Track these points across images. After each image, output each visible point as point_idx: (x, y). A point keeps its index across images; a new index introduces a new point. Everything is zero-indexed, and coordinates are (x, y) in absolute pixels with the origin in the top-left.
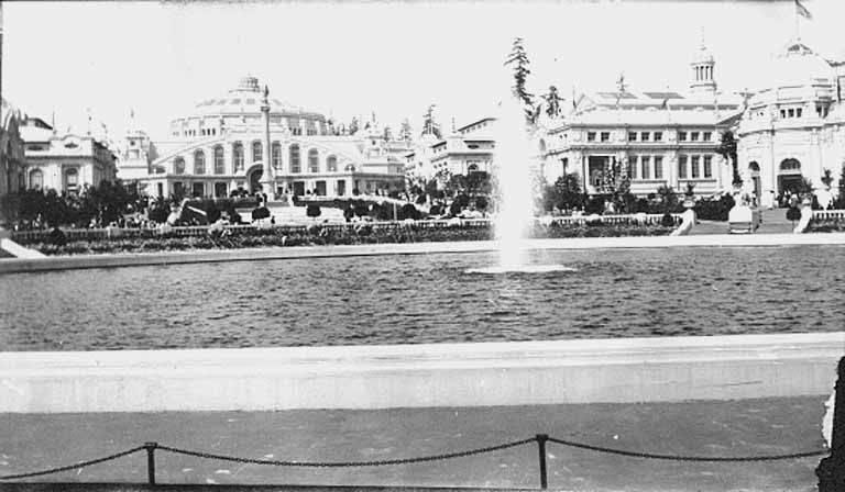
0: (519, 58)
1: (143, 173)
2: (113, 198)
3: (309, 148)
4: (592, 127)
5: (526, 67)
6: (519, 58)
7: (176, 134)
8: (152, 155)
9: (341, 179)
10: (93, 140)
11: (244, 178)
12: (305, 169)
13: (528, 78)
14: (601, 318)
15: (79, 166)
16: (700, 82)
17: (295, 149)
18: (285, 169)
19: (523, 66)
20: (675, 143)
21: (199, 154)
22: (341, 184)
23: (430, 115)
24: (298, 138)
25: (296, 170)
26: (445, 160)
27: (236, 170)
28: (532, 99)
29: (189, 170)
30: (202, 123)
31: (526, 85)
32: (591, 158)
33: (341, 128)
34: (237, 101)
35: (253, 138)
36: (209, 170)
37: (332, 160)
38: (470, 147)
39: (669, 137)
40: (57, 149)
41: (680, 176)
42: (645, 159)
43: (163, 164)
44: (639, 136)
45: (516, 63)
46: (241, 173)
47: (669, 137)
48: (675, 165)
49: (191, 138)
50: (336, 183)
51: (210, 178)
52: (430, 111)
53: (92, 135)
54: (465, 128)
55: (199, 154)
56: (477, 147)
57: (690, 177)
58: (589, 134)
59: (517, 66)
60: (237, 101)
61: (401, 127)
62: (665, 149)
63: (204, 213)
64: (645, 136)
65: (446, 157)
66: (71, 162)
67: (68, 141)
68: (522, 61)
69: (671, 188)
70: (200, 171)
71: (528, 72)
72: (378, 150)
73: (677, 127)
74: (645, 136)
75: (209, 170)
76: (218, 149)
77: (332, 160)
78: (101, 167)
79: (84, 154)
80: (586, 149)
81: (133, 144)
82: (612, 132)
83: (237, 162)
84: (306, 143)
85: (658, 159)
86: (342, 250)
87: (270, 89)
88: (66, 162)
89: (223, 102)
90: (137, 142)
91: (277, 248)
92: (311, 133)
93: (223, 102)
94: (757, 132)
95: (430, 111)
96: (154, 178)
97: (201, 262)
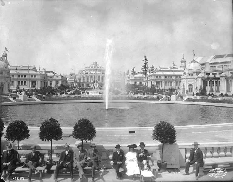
1: (73, 82)
2: (64, 87)
5: (147, 61)
7: (80, 73)
8: (75, 78)
16: (182, 65)
20: (164, 79)
21: (84, 78)
29: (82, 81)
30: (85, 71)
31: (147, 65)
34: (92, 67)
35: (91, 75)
38: (95, 76)
40: (55, 78)
41: (176, 86)
42: (169, 82)
45: (145, 61)
46: (92, 82)
47: (163, 78)
48: (175, 84)
49: (82, 75)
52: (134, 69)
55: (84, 78)
57: (178, 86)
58: (31, 76)
60: (92, 67)
62: (173, 80)
64: (22, 76)
66: (57, 80)
67: (57, 76)
71: (147, 63)
73: (165, 75)
74: (22, 76)
76: (88, 77)
80: (155, 80)
83: (91, 79)
85: (171, 82)
87: (195, 54)
88: (56, 80)
89: (90, 67)
93: (90, 67)
94: (194, 78)
95: (134, 69)
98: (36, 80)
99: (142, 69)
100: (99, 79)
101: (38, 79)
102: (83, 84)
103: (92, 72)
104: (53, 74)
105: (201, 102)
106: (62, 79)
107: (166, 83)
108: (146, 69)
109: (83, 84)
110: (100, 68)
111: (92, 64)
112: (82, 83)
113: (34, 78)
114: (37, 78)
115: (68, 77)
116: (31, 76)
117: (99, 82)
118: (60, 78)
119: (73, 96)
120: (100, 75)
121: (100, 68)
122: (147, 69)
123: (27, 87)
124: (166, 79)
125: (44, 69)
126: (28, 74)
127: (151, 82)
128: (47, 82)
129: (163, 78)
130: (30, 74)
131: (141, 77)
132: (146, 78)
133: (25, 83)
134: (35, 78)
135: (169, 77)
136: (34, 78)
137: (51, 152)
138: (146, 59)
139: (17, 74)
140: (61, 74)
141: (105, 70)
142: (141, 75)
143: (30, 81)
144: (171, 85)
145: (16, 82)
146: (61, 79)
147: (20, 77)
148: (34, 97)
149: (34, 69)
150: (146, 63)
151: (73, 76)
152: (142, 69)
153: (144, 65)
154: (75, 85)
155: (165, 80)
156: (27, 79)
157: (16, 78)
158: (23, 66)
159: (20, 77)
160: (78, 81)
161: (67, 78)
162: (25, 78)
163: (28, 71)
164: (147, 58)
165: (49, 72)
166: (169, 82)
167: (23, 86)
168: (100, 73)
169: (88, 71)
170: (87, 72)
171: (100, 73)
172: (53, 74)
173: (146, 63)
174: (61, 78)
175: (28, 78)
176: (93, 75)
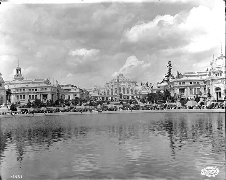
3: (135, 90)
4: (20, 88)
5: (171, 68)
12: (130, 94)
14: (33, 150)
15: (77, 94)
18: (126, 94)
29: (107, 94)
31: (171, 72)
32: (180, 89)
36: (110, 94)
37: (135, 91)
39: (26, 91)
40: (72, 91)
42: (195, 89)
45: (169, 67)
47: (188, 84)
51: (110, 96)
53: (79, 88)
64: (21, 90)
68: (171, 67)
70: (108, 94)
71: (172, 69)
73: (189, 81)
75: (110, 94)
76: (112, 89)
77: (135, 91)
79: (77, 91)
82: (185, 82)
88: (74, 93)
90: (96, 89)
91: (148, 110)
98: (47, 94)
100: (124, 92)
101: (77, 92)
102: (107, 97)
105: (189, 75)
106: (52, 91)
107: (191, 89)
110: (125, 80)
114: (47, 91)
117: (124, 94)
120: (125, 87)
124: (191, 85)
126: (38, 87)
129: (188, 84)
130: (40, 87)
133: (20, 98)
134: (46, 91)
135: (195, 83)
136: (44, 91)
138: (170, 65)
139: (28, 88)
144: (195, 92)
145: (27, 96)
146: (79, 92)
147: (31, 91)
150: (170, 70)
153: (168, 71)
155: (190, 87)
156: (37, 93)
157: (27, 92)
159: (31, 91)
160: (103, 95)
162: (36, 91)
163: (38, 84)
164: (171, 63)
165: (63, 86)
166: (195, 89)
167: (22, 100)
169: (113, 84)
170: (112, 84)
173: (170, 70)
174: (78, 91)
175: (39, 91)
176: (126, 87)
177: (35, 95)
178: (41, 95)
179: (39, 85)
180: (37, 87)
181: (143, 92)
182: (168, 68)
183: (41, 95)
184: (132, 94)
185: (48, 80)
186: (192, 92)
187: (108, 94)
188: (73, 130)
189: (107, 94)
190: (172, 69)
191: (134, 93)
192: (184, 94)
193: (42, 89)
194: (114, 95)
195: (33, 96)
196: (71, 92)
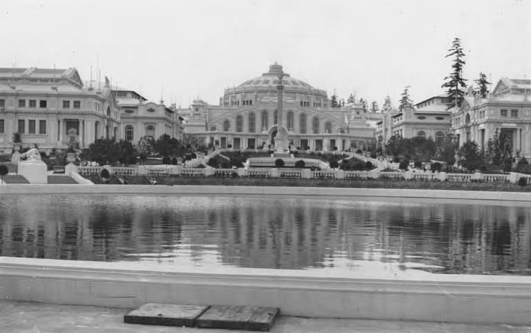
0: (457, 52)
1: (203, 131)
3: (313, 115)
6: (457, 52)
9: (224, 136)
10: (164, 106)
11: (267, 136)
12: (310, 132)
13: (464, 67)
17: (303, 117)
18: (296, 131)
19: (460, 58)
22: (333, 142)
23: (406, 93)
24: (306, 108)
25: (303, 131)
26: (401, 127)
27: (262, 130)
28: (466, 83)
33: (342, 102)
34: (267, 82)
35: (261, 108)
38: (126, 111)
40: (141, 112)
43: (215, 124)
44: (72, 104)
45: (455, 57)
46: (265, 132)
49: (235, 107)
50: (329, 142)
54: (420, 104)
55: (239, 120)
56: (424, 118)
58: (64, 102)
59: (456, 58)
61: (384, 102)
63: (228, 159)
64: (32, 103)
65: (402, 125)
68: (460, 56)
69: (134, 146)
71: (464, 63)
72: (199, 115)
74: (32, 103)
78: (171, 125)
80: (499, 123)
81: (358, 113)
84: (311, 113)
86: (314, 200)
90: (201, 109)
92: (316, 105)
93: (258, 82)
95: (406, 90)
96: (208, 134)
97: (36, 194)
98: (80, 118)
99: (446, 85)
100: (290, 125)
102: (317, 141)
103: (266, 99)
104: (135, 102)
108: (459, 85)
109: (237, 141)
111: (267, 71)
112: (233, 135)
113: (71, 108)
115: (185, 115)
116: (64, 102)
117: (291, 133)
118: (162, 113)
119: (209, 171)
120: (294, 109)
121: (292, 85)
122: (463, 85)
123: (55, 138)
125: (107, 79)
127: (483, 131)
128: (115, 125)
130: (59, 96)
131: (440, 116)
132: (463, 117)
137: (85, 170)
138: (459, 52)
140: (162, 102)
141: (76, 75)
142: (441, 108)
143: (59, 122)
146: (164, 119)
148: (71, 170)
149: (75, 79)
150: (458, 67)
151: (199, 106)
152: (446, 85)
154: (208, 141)
158: (37, 71)
161: (184, 118)
162: (43, 110)
165: (123, 94)
168: (292, 101)
171: (292, 101)
172: (135, 102)
173: (458, 67)
177: (41, 121)
178: (61, 123)
179: (54, 88)
180: (48, 95)
181: (353, 129)
182: (452, 60)
183: (61, 123)
184: (316, 131)
185: (76, 72)
186: (34, 128)
187: (239, 130)
188: (86, 234)
189: (233, 129)
190: (464, 63)
191: (322, 132)
192: (139, 140)
193: (66, 104)
194: (257, 133)
195: (32, 123)
196: (136, 118)
